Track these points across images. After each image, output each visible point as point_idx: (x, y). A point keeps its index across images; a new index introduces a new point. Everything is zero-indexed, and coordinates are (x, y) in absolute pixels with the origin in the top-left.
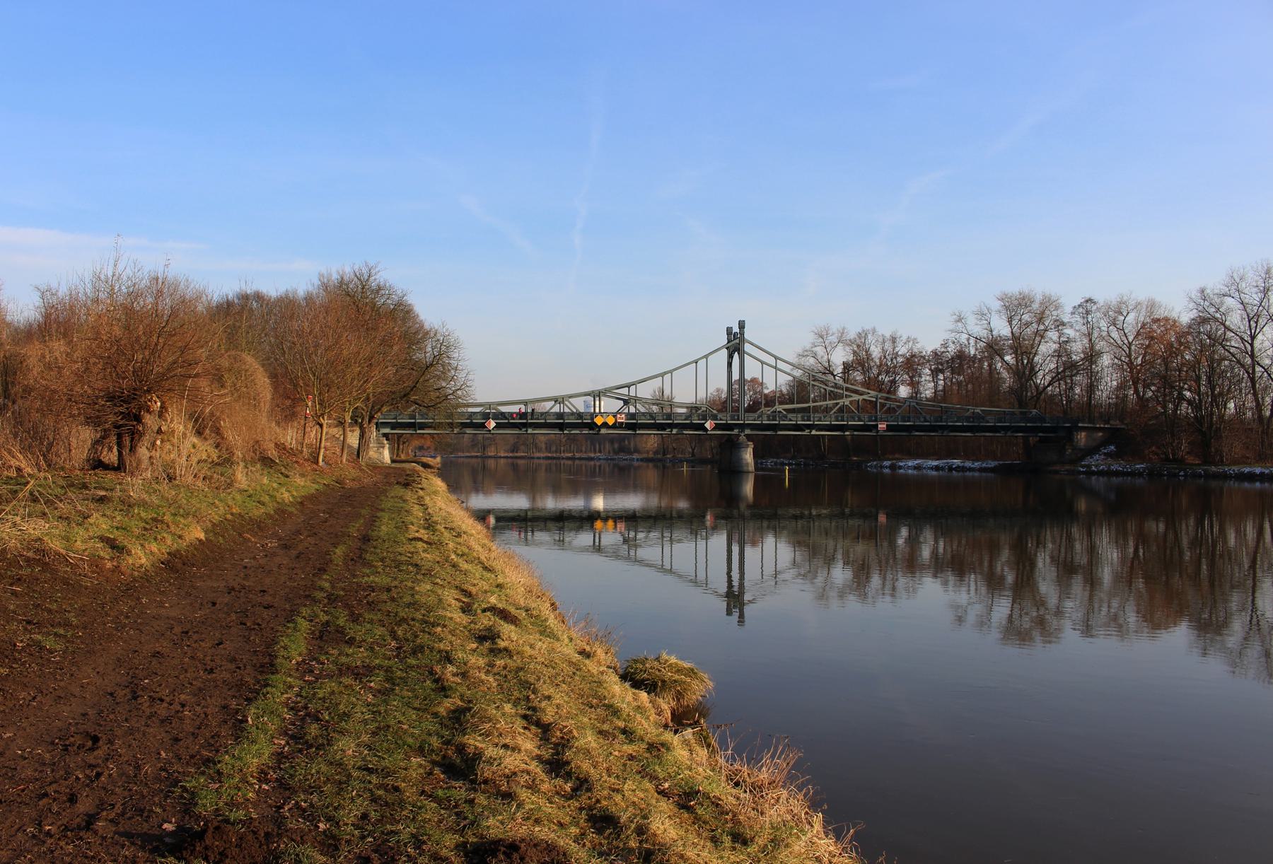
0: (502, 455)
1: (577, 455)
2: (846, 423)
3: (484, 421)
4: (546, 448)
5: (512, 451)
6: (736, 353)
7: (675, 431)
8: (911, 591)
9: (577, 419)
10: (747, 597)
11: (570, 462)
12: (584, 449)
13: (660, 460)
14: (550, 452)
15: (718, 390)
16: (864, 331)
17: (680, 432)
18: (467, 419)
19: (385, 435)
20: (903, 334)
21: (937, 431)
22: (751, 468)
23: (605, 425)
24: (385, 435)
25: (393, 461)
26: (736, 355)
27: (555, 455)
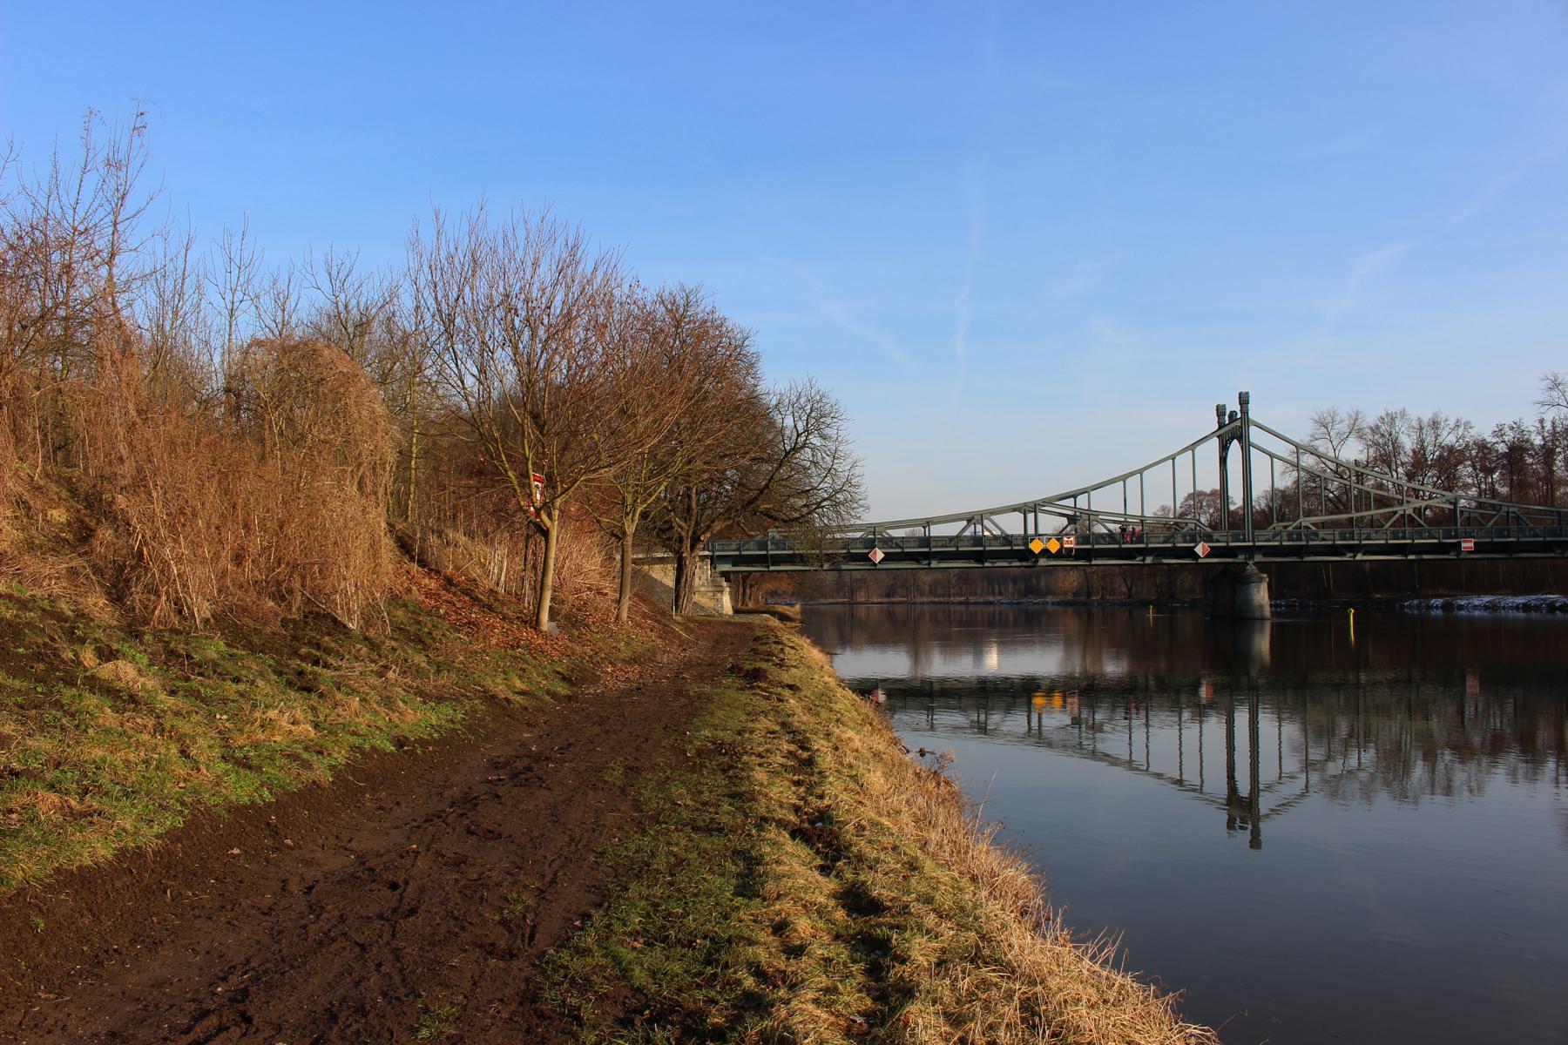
0: (875, 601)
1: (973, 599)
2: (1410, 541)
3: (867, 551)
4: (931, 590)
5: (888, 596)
6: (1235, 442)
7: (1149, 560)
8: (1476, 790)
9: (1004, 545)
10: (1265, 803)
11: (962, 608)
12: (979, 591)
13: (1084, 604)
14: (935, 596)
15: (1163, 509)
16: (1387, 414)
17: (1157, 561)
18: (842, 549)
19: (725, 574)
20: (1450, 414)
21: (1554, 551)
22: (1267, 611)
23: (1045, 553)
24: (725, 574)
25: (737, 611)
26: (1235, 447)
27: (942, 600)
